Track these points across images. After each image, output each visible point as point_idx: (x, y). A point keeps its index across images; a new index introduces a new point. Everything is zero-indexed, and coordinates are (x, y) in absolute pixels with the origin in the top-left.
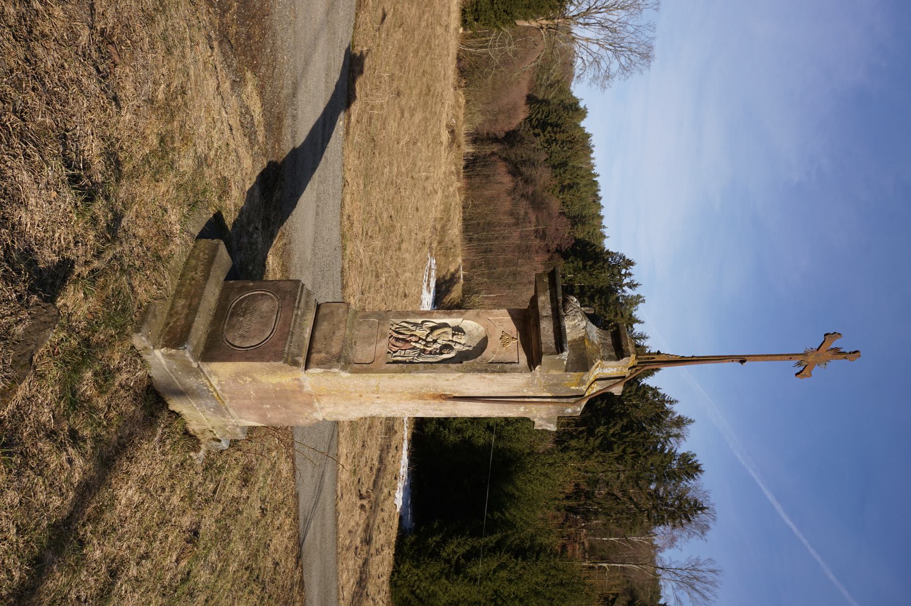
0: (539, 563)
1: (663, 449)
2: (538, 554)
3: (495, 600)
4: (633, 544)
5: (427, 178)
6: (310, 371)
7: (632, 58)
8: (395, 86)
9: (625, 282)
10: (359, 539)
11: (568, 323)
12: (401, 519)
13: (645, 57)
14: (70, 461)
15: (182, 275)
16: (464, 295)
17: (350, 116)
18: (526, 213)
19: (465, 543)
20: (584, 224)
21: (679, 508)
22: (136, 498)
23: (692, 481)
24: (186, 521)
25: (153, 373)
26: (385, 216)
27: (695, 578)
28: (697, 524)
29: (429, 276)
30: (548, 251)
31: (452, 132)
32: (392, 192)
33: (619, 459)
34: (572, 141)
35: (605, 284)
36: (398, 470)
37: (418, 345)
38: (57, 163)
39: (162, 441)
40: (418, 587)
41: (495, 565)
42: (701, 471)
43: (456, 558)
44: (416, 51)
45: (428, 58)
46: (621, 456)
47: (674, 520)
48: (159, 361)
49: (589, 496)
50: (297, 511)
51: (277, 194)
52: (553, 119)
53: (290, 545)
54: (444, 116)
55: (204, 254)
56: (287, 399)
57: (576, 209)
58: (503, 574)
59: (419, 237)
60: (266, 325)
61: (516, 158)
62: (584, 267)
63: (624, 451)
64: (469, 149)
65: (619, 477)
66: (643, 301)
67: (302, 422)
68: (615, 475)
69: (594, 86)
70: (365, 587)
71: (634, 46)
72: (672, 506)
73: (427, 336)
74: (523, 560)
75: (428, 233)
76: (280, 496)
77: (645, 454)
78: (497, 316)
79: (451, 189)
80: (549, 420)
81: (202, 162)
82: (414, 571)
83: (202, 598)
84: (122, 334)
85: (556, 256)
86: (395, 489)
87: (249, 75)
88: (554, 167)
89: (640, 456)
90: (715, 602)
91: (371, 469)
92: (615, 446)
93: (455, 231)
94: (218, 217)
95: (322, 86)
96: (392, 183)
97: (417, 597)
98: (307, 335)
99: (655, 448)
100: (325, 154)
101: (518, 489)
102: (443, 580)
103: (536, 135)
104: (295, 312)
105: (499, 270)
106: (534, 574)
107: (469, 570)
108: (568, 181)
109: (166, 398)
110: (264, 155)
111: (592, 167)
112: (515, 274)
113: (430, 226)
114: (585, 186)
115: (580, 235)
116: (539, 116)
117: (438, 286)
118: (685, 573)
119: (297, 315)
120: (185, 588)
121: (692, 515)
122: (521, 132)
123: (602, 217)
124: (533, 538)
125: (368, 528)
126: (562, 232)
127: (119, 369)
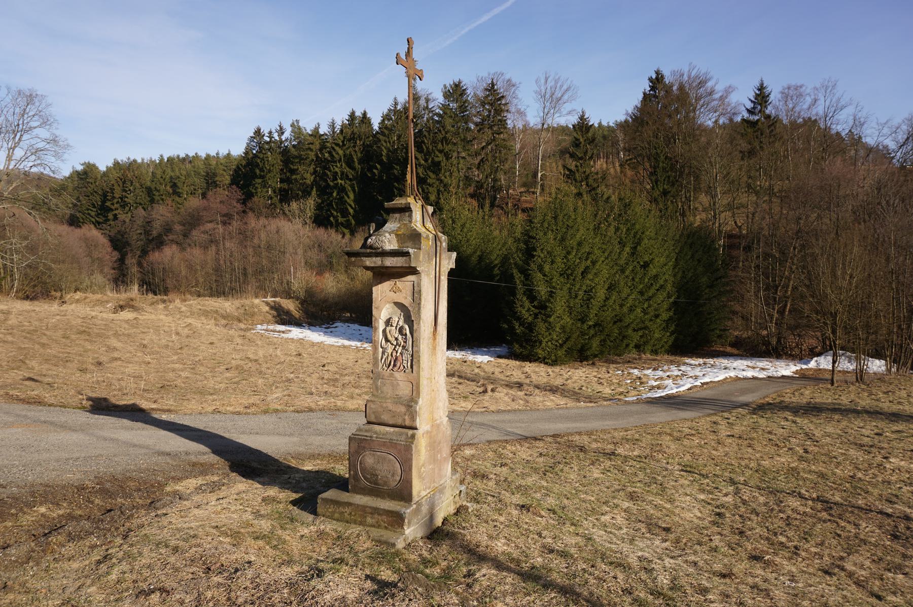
1: (438, 115)
2: (531, 237)
3: (568, 276)
4: (522, 148)
5: (177, 334)
6: (418, 426)
7: (31, 114)
8: (92, 367)
9: (277, 138)
10: (519, 393)
11: (388, 247)
12: (500, 357)
13: (32, 100)
14: (484, 576)
15: (347, 522)
16: (292, 298)
17: (153, 409)
18: (203, 232)
20: (215, 175)
21: (491, 105)
22: (503, 541)
23: (468, 92)
24: (515, 512)
25: (419, 535)
26: (228, 375)
27: (551, 96)
28: (506, 90)
29: (274, 331)
30: (244, 212)
31: (122, 308)
32: (202, 369)
33: (448, 157)
34: (124, 181)
35: (279, 157)
36: (458, 360)
38: (313, 583)
39: (464, 528)
40: (557, 341)
41: (539, 275)
42: (460, 82)
44: (43, 345)
45: (48, 333)
46: (445, 155)
47: (502, 111)
48: (412, 531)
49: (479, 185)
50: (500, 441)
51: (255, 465)
52: (98, 199)
53: (528, 445)
54: (105, 315)
56: (435, 442)
57: (199, 182)
58: (547, 268)
59: (239, 341)
60: (385, 459)
61: (141, 240)
62: (262, 177)
63: (441, 151)
64: (134, 291)
65: (464, 158)
66: (297, 121)
67: (449, 432)
68: (462, 161)
69: (66, 156)
70: (557, 388)
71: (17, 110)
72: (490, 111)
75: (232, 332)
76: (490, 454)
77: (443, 132)
79: (184, 309)
80: (450, 258)
81: (257, 515)
82: (544, 345)
83: (566, 501)
84: (397, 554)
85: (249, 205)
86: (475, 362)
87: (168, 489)
88: (152, 201)
89: (445, 137)
91: (460, 384)
92: (436, 159)
93: (227, 305)
94: (294, 503)
95: (144, 432)
96: (193, 369)
97: (565, 342)
98: (392, 429)
99: (437, 122)
100: (202, 428)
101: (475, 252)
102: (551, 320)
103: (115, 217)
105: (264, 262)
106: (547, 241)
108: (168, 188)
109: (435, 527)
110: (228, 476)
111: (152, 162)
112: (269, 248)
113: (225, 331)
114: (173, 171)
115: (227, 180)
116: (93, 214)
117: (283, 323)
118: (548, 104)
120: (559, 512)
121: (498, 94)
122: (112, 234)
123: (208, 156)
124: (517, 240)
125: (509, 386)
126: (223, 197)
127: (420, 555)
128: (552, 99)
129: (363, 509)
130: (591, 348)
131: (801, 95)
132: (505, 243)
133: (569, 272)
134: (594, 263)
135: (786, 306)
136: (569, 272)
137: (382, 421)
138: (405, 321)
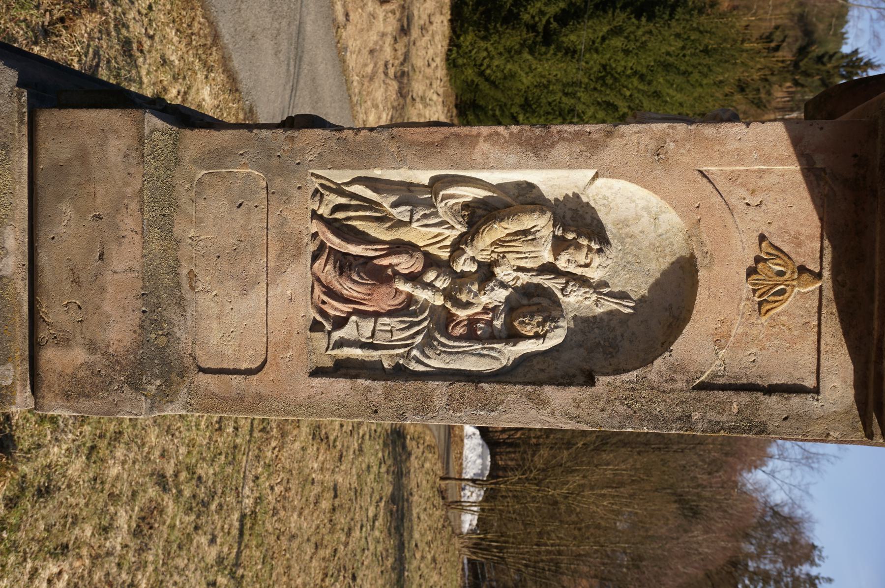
0: (673, 23)
37: (422, 295)
40: (489, 66)
41: (605, 29)
43: (544, 21)
58: (617, 42)
73: (457, 248)
74: (649, 20)
78: (740, 156)
82: (483, 44)
97: (487, 79)
102: (526, 55)
107: (564, 39)
133: (609, 81)
136: (609, 81)
137: (44, 210)
138: (585, 325)
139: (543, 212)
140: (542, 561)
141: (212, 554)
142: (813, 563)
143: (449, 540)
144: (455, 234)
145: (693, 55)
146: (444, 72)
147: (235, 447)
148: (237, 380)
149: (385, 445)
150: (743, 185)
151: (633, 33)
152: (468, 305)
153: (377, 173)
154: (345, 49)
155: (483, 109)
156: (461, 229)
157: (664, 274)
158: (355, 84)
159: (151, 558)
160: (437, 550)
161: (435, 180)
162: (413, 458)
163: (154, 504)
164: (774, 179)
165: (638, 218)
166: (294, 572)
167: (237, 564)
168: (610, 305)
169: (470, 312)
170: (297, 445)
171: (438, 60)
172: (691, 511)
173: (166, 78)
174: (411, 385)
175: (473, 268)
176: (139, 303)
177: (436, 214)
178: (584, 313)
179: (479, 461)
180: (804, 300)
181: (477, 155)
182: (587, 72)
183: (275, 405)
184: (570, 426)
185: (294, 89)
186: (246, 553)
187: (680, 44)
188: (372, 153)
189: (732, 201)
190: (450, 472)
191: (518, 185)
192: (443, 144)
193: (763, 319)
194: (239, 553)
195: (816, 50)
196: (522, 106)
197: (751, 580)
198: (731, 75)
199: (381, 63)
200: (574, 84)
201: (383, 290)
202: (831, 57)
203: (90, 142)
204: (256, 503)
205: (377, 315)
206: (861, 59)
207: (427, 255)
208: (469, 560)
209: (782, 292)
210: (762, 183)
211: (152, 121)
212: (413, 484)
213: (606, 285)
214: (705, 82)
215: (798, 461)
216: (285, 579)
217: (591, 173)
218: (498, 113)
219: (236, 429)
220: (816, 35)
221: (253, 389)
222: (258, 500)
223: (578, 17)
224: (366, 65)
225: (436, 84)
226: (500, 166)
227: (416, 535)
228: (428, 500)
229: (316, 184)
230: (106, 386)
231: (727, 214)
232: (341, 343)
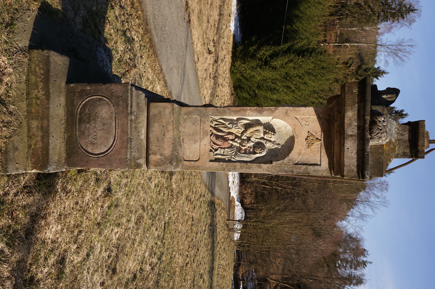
0: (311, 58)
2: (311, 53)
3: (286, 77)
12: (234, 36)
15: (28, 94)
19: (270, 49)
37: (235, 144)
40: (245, 73)
41: (287, 60)
55: (40, 68)
58: (291, 65)
72: (394, 9)
73: (242, 133)
74: (302, 57)
78: (304, 114)
82: (243, 65)
90: (407, 62)
97: (244, 78)
98: (143, 136)
101: (301, 12)
104: (130, 118)
106: (308, 64)
107: (272, 64)
118: (394, 48)
119: (131, 120)
121: (406, 15)
128: (397, 51)
129: (45, 116)
130: (242, 92)
131: (382, 191)
132: (306, 32)
134: (293, 91)
135: (267, 185)
136: (288, 78)
137: (151, 124)
138: (271, 151)
139: (261, 126)
140: (263, 251)
141: (156, 234)
142: (364, 256)
143: (230, 242)
144: (242, 130)
145: (318, 69)
146: (229, 75)
147: (163, 200)
148: (193, 163)
149: (208, 206)
150: (304, 120)
151: (297, 61)
152: (245, 146)
153: (225, 117)
154: (198, 70)
155: (243, 88)
156: (243, 129)
157: (288, 139)
158: (200, 81)
159: (140, 232)
160: (226, 245)
161: (237, 119)
162: (217, 211)
163: (141, 215)
164: (311, 119)
165: (282, 127)
166: (180, 244)
167: (163, 238)
168: (276, 146)
169: (245, 148)
170: (181, 202)
171: (227, 71)
172: (318, 235)
173: (148, 84)
174: (232, 164)
175: (246, 138)
176: (172, 145)
177: (238, 126)
178: (270, 148)
179: (241, 215)
180: (318, 146)
181: (247, 113)
182: (280, 75)
183: (201, 168)
184: (267, 173)
185: (182, 85)
186: (166, 235)
187: (314, 65)
188: (224, 113)
189: (302, 124)
190: (230, 218)
191: (256, 120)
192: (239, 111)
193: (309, 149)
194: (164, 235)
195: (364, 67)
196: (257, 87)
197: (341, 262)
198: (332, 77)
199: (209, 74)
200: (275, 79)
201: (226, 143)
202: (370, 69)
203: (162, 110)
204: (169, 219)
205: (224, 148)
206: (381, 70)
207: (235, 135)
208: (237, 250)
209: (313, 144)
210: (309, 120)
211: (176, 105)
212: (217, 221)
213: (275, 142)
214: (323, 79)
215: (358, 217)
216: (177, 246)
217: (272, 117)
218: (248, 89)
219: (164, 194)
220: (365, 61)
221: (196, 165)
222: (170, 218)
223: (277, 56)
224: (204, 75)
225: (226, 79)
226: (252, 116)
227: (218, 239)
228: (222, 227)
229: (211, 119)
230: (164, 164)
231: (301, 127)
232: (216, 155)
